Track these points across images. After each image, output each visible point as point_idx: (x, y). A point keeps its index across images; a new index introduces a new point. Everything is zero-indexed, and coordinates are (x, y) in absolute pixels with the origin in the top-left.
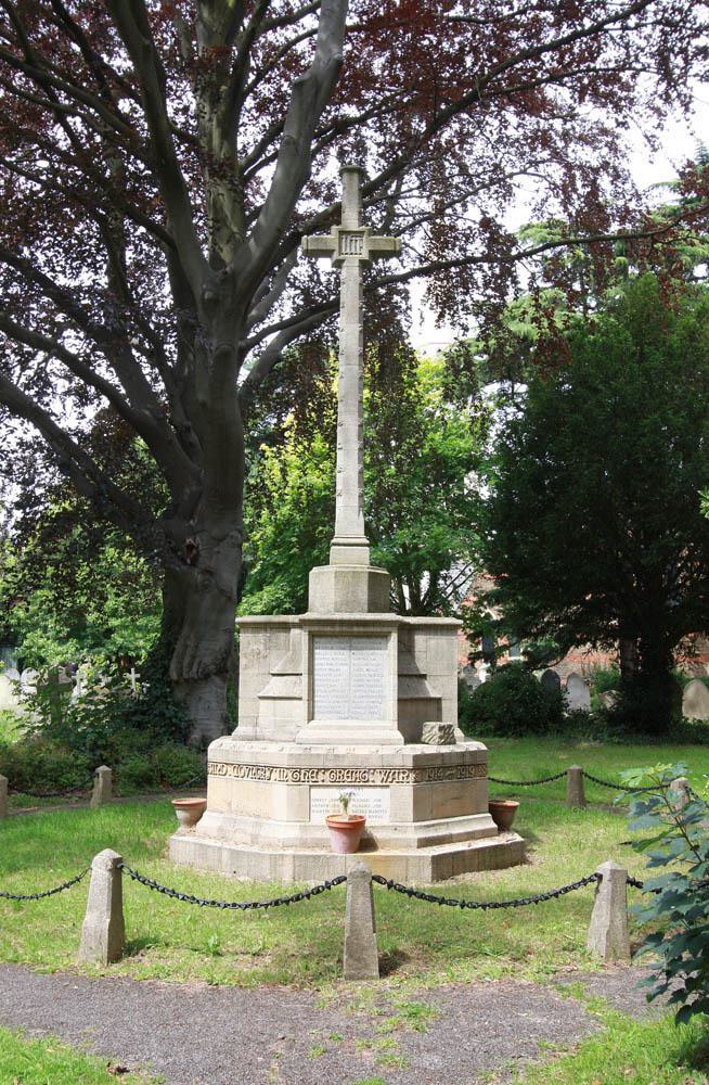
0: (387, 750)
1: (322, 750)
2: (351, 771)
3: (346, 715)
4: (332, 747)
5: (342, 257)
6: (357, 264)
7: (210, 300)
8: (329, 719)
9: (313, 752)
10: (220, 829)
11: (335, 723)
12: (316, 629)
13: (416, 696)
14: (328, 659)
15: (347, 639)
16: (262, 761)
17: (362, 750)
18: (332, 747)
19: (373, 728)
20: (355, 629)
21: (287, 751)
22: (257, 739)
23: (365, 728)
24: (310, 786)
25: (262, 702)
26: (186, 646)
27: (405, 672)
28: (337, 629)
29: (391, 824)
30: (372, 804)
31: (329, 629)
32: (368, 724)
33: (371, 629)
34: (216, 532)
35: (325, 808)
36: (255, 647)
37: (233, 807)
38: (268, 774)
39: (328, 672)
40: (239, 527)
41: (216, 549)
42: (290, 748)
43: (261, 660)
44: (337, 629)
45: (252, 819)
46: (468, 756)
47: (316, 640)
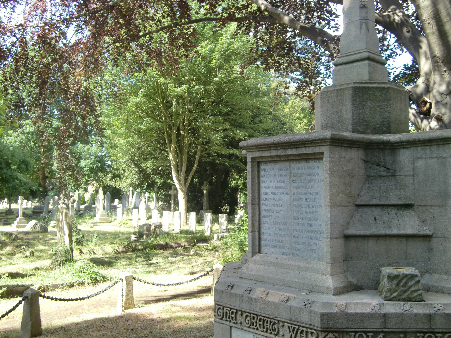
3: (287, 251)
14: (272, 188)
15: (287, 164)
39: (272, 202)
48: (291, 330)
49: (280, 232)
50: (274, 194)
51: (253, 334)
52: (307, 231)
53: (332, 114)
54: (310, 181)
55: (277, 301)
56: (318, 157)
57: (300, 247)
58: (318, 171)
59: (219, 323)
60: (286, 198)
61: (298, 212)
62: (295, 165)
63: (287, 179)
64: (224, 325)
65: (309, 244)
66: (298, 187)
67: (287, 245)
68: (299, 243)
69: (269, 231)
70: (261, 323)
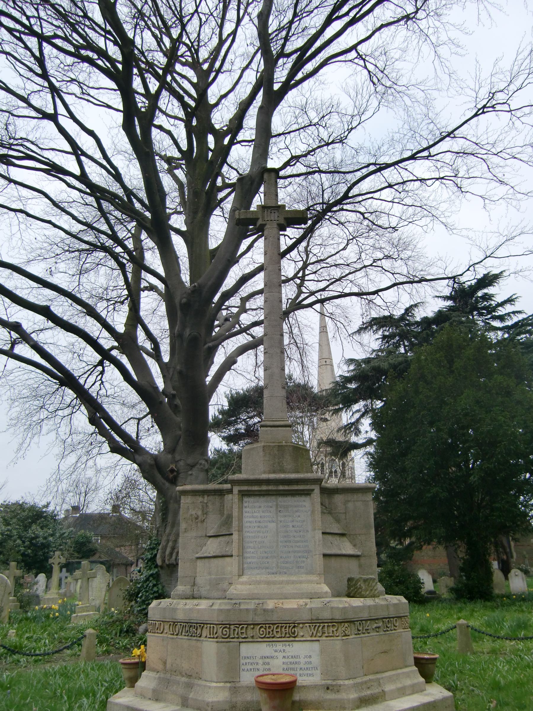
0: (316, 604)
1: (251, 605)
2: (280, 625)
3: (275, 570)
4: (261, 601)
5: (264, 223)
6: (276, 226)
7: (185, 304)
8: (258, 574)
9: (243, 607)
10: (154, 691)
11: (264, 577)
12: (245, 488)
13: (339, 552)
14: (257, 517)
15: (273, 498)
16: (195, 617)
17: (291, 604)
18: (261, 601)
19: (301, 582)
20: (281, 488)
21: (216, 607)
22: (194, 598)
23: (293, 582)
24: (240, 642)
25: (199, 563)
26: (168, 541)
27: (328, 531)
28: (264, 488)
29: (323, 682)
30: (302, 660)
31: (256, 488)
32: (294, 578)
33: (295, 487)
34: (190, 461)
35: (255, 666)
36: (194, 513)
37: (168, 666)
38: (199, 631)
39: (256, 529)
40: (206, 457)
41: (190, 472)
42: (218, 605)
43: (199, 524)
44: (264, 488)
45: (184, 679)
46: (391, 609)
47: (246, 499)
48: (313, 628)
49: (266, 555)
50: (259, 522)
51: (268, 643)
52: (295, 552)
53: (274, 464)
54: (297, 511)
55: (296, 606)
56: (307, 493)
57: (287, 565)
58: (304, 503)
59: (224, 642)
60: (273, 525)
61: (285, 537)
62: (280, 499)
63: (273, 509)
64: (231, 644)
65: (297, 562)
66: (285, 516)
67: (274, 565)
68: (287, 563)
69: (254, 555)
70: (279, 630)
